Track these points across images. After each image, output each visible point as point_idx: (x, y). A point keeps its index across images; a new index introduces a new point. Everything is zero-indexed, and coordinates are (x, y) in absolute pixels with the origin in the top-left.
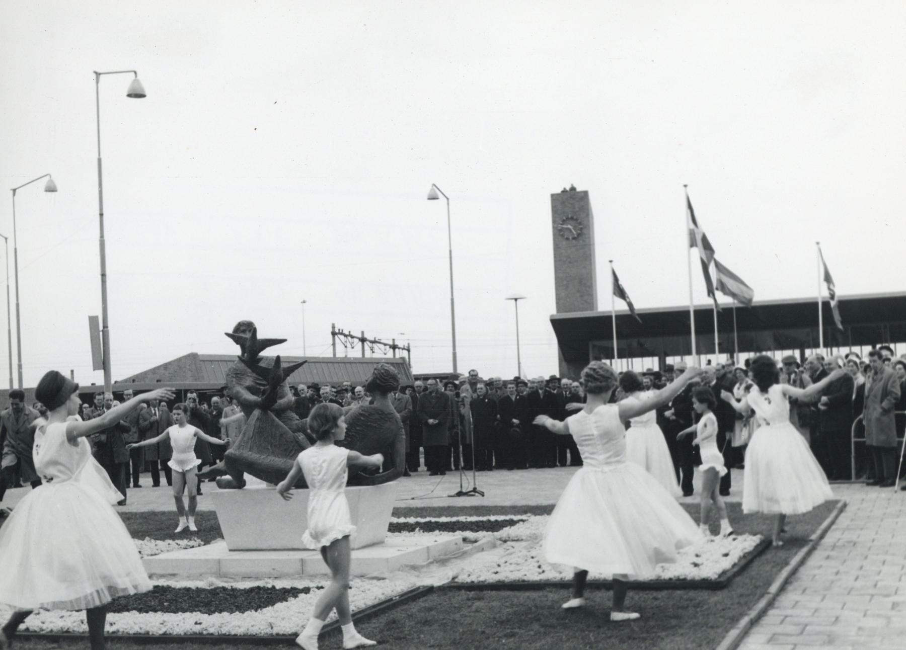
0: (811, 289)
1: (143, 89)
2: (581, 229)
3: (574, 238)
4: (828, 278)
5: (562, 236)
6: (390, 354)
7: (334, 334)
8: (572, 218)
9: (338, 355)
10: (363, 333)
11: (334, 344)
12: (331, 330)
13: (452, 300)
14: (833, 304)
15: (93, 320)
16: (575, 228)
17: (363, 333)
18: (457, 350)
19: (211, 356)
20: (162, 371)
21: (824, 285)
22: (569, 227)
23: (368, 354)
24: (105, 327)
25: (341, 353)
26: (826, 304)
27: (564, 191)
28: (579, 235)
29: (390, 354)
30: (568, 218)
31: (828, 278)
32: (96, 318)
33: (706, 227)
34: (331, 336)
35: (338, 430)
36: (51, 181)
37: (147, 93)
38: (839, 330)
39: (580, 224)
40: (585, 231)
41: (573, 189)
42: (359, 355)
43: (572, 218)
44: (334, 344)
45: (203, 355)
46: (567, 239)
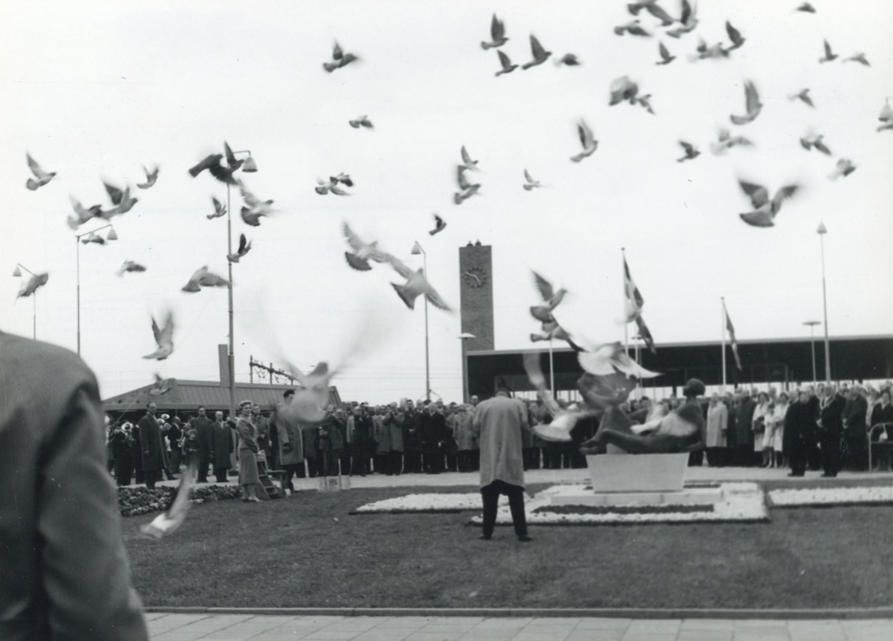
0: (709, 332)
1: (255, 166)
2: (485, 279)
3: (479, 286)
4: (730, 327)
5: (468, 284)
6: (289, 383)
7: (252, 364)
8: (477, 269)
9: (254, 382)
10: (271, 364)
11: (251, 374)
12: (249, 361)
13: (79, 333)
14: (734, 347)
15: (222, 348)
16: (479, 277)
17: (271, 364)
18: (430, 380)
19: (209, 382)
20: (141, 394)
21: (727, 333)
22: (475, 276)
23: (274, 382)
24: (232, 353)
25: (256, 380)
26: (728, 347)
27: (470, 245)
28: (483, 283)
29: (289, 383)
30: (474, 269)
31: (730, 327)
32: (225, 346)
33: (638, 281)
34: (249, 367)
35: (664, 424)
36: (112, 231)
37: (258, 168)
38: (738, 370)
39: (484, 274)
40: (488, 280)
41: (478, 244)
42: (268, 382)
43: (477, 269)
44: (251, 374)
45: (180, 381)
46: (473, 287)
